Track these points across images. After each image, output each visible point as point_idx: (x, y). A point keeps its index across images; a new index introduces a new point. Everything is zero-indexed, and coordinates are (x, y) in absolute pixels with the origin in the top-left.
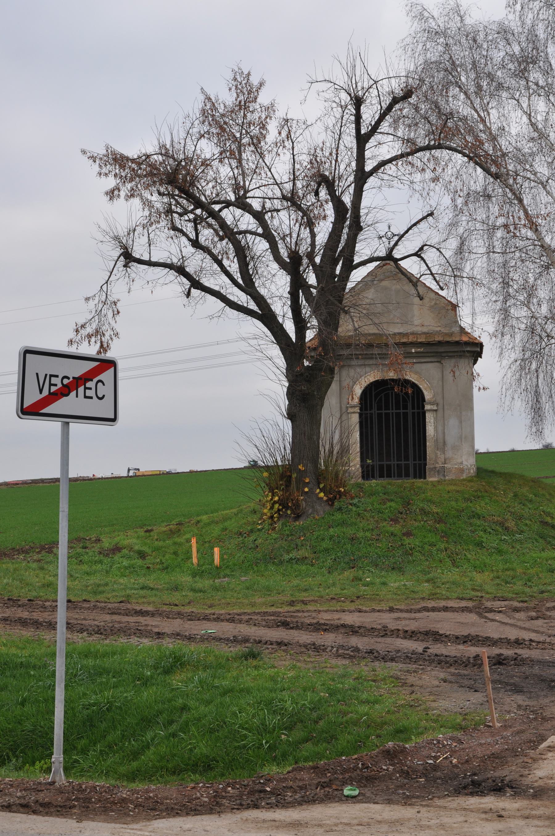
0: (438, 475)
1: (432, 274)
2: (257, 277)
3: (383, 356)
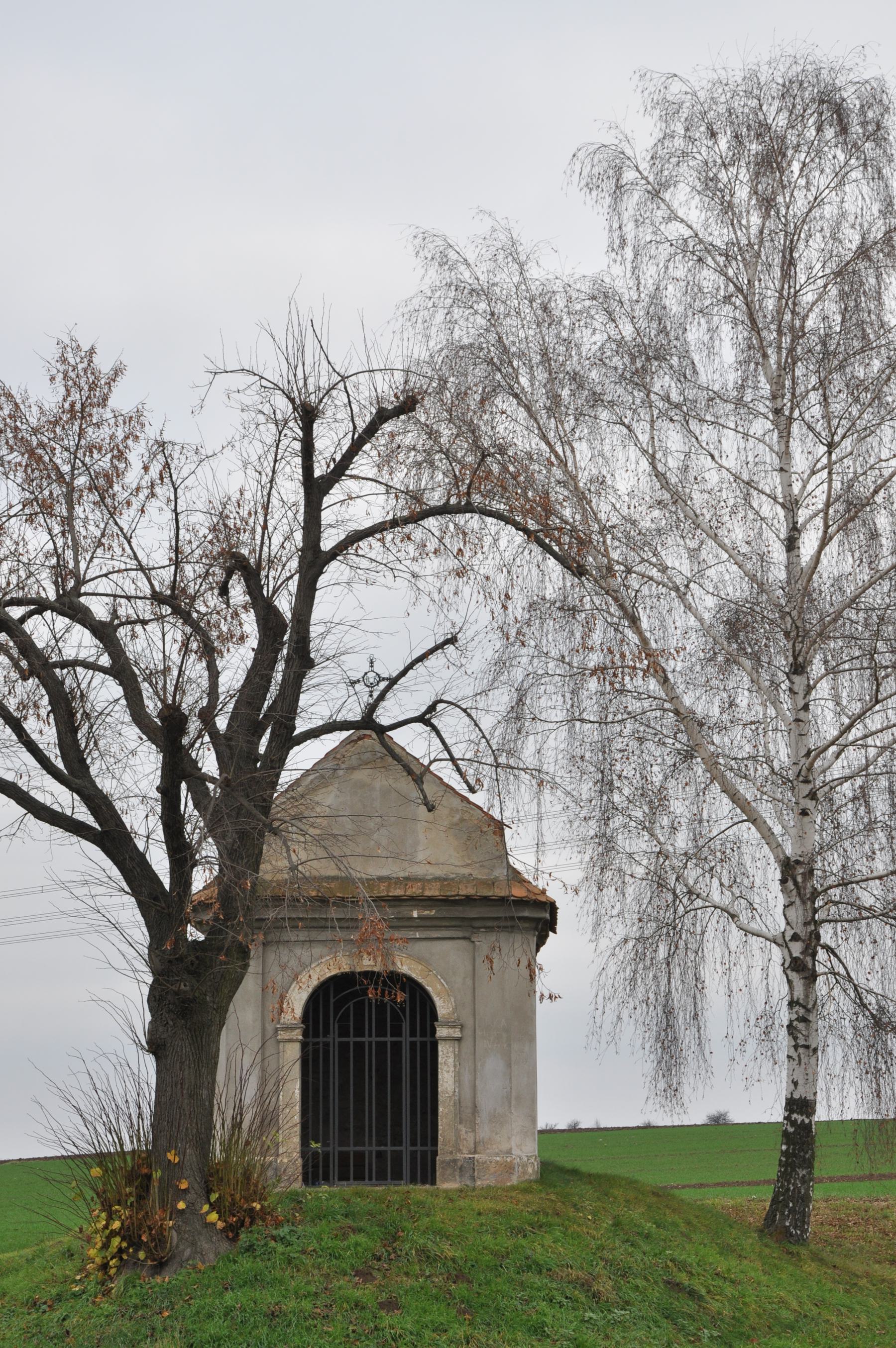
0: (461, 1176)
1: (452, 759)
2: (96, 754)
3: (349, 924)
